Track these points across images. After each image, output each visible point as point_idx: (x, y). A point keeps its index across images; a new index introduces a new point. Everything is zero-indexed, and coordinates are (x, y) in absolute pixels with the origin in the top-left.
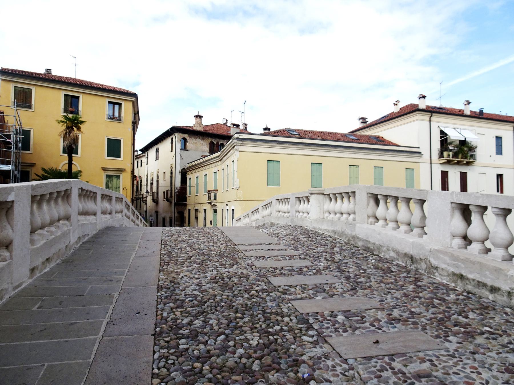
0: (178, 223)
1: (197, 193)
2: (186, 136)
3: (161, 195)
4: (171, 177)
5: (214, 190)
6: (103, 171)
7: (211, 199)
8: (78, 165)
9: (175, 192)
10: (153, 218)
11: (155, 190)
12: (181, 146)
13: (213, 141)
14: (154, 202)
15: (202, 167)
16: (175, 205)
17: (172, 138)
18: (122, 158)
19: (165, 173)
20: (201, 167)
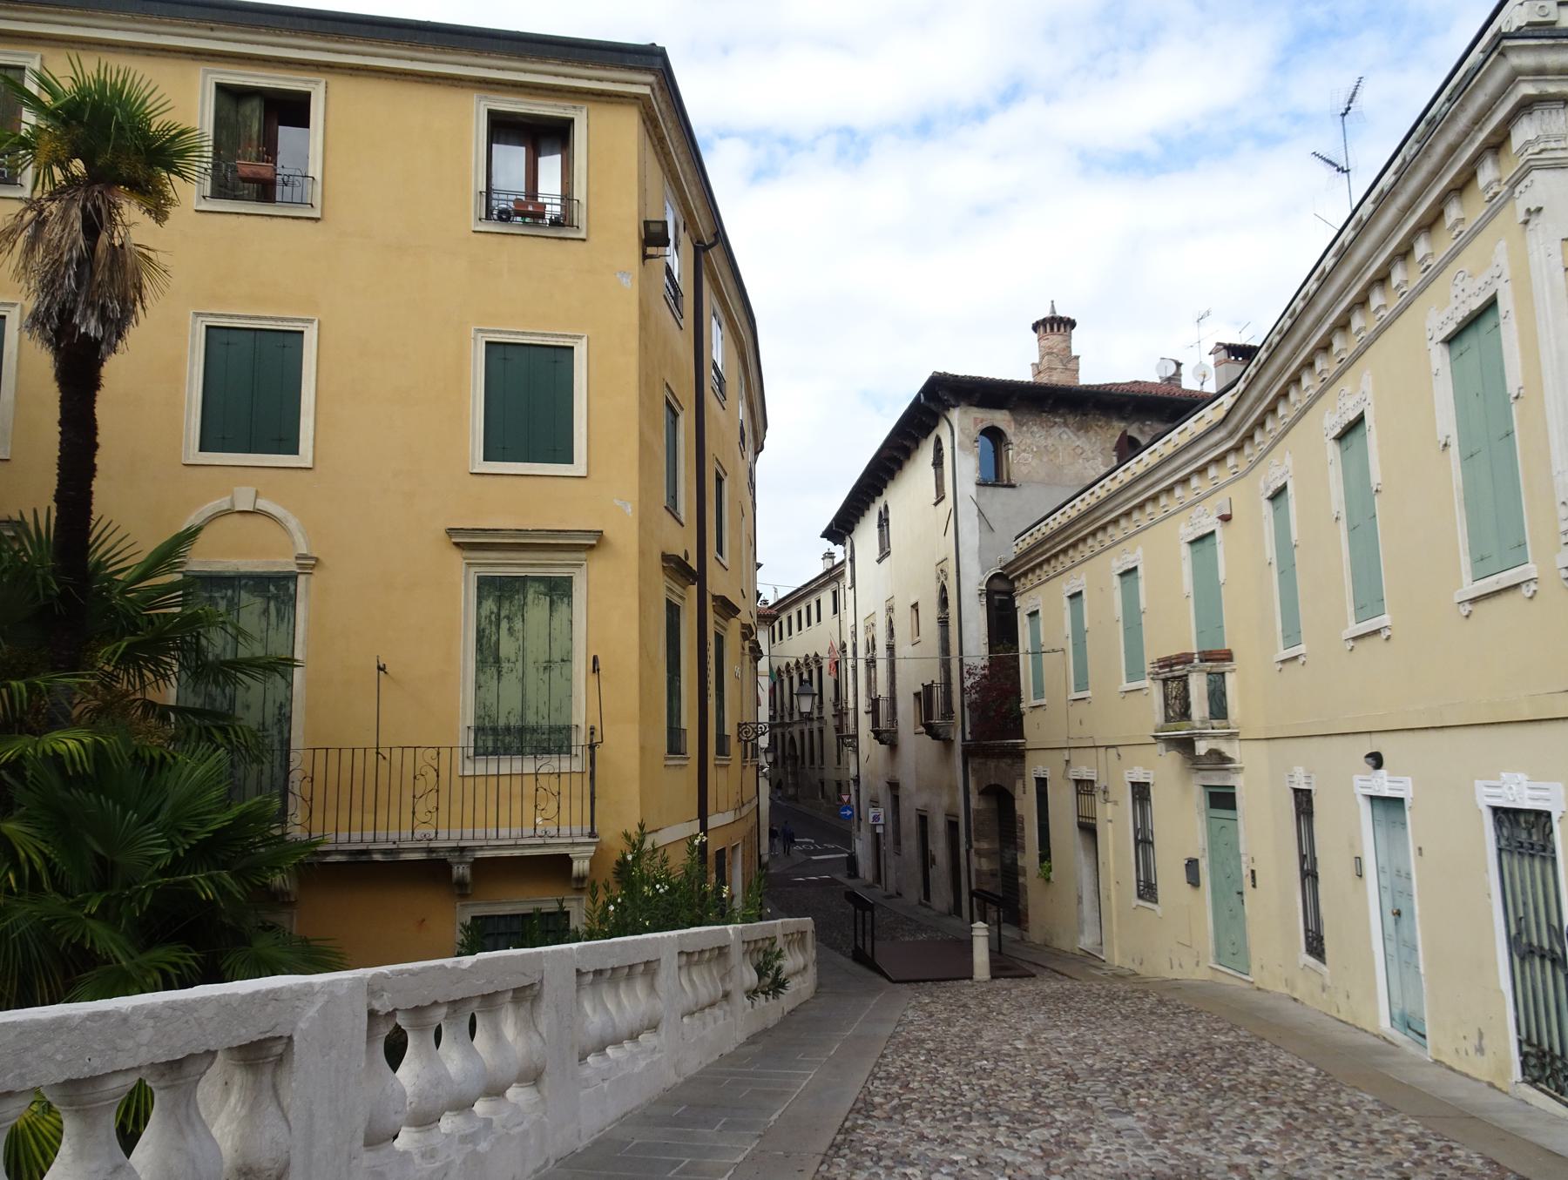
0: (985, 845)
1: (1081, 684)
2: (1001, 419)
3: (907, 709)
4: (944, 623)
5: (1206, 657)
6: (457, 557)
7: (1185, 714)
8: (293, 523)
9: (963, 690)
10: (881, 810)
11: (882, 690)
12: (982, 468)
13: (1133, 431)
14: (882, 742)
15: (1104, 528)
16: (968, 753)
17: (938, 441)
18: (579, 467)
19: (915, 606)
20: (1093, 534)
